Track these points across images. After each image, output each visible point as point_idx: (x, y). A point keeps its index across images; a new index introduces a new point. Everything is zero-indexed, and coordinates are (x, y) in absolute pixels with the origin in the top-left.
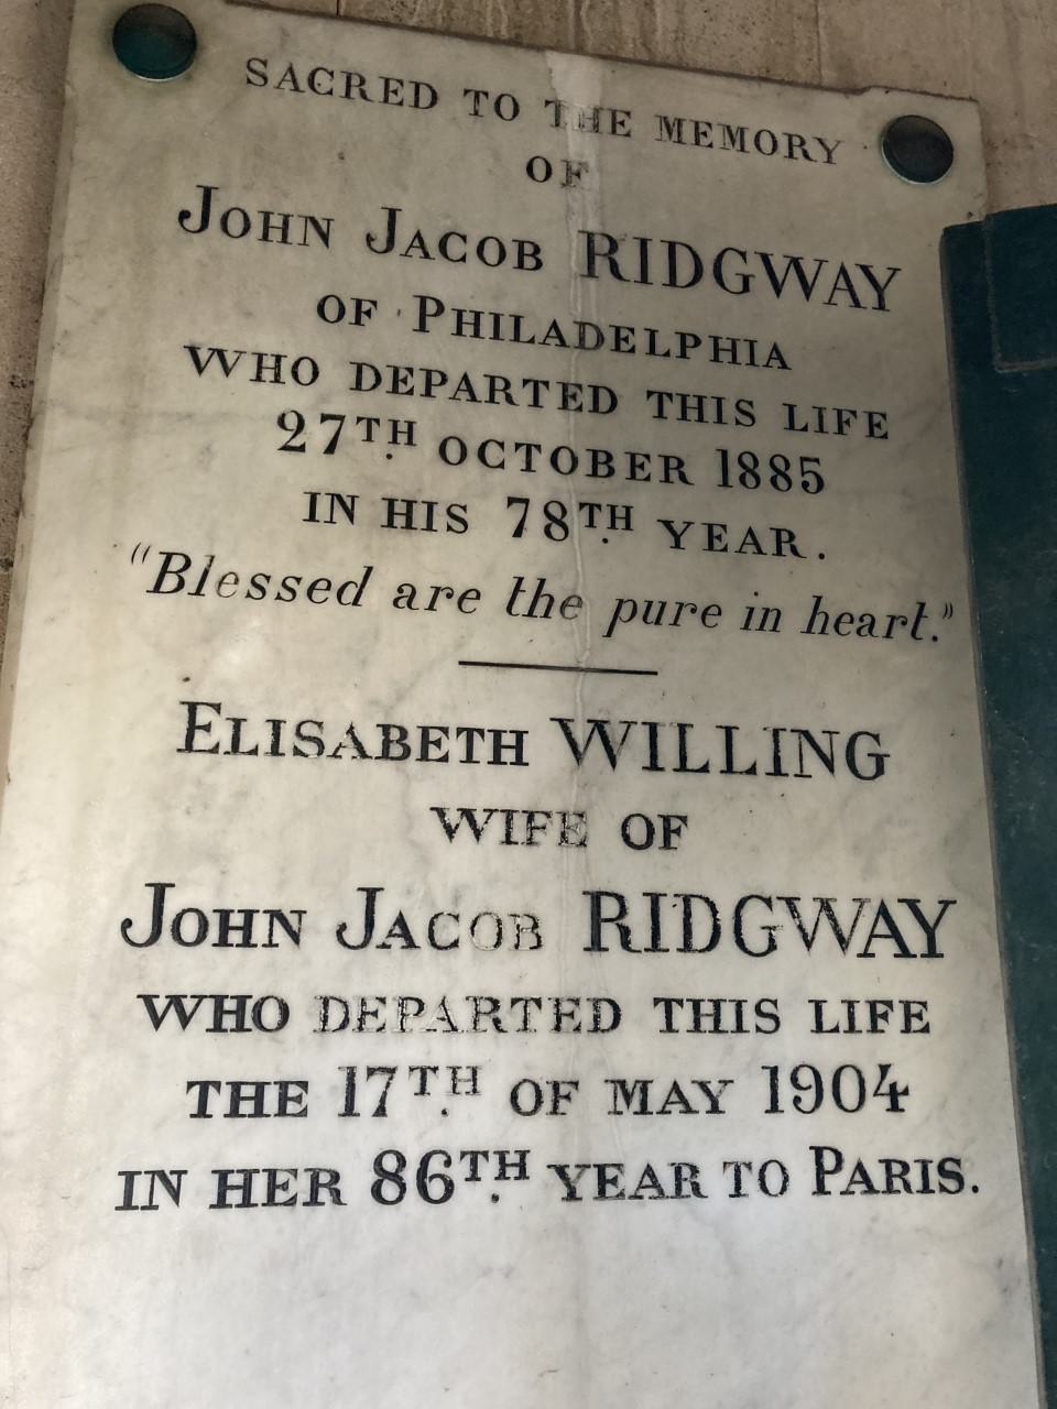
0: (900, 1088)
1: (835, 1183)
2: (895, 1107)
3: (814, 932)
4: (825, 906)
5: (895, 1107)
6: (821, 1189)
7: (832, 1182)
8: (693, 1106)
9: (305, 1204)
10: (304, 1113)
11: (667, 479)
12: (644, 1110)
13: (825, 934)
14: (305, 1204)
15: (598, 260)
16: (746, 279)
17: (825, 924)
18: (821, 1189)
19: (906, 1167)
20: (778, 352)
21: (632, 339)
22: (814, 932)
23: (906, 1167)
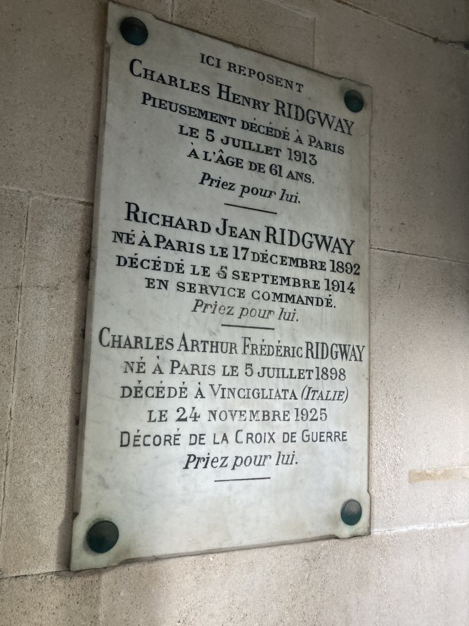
0: (198, 415)
1: (177, 371)
2: (352, 292)
3: (332, 122)
4: (327, 116)
5: (352, 292)
6: (172, 372)
7: (175, 370)
8: (343, 251)
9: (158, 421)
10: (166, 420)
11: (268, 241)
12: (293, 302)
13: (326, 123)
14: (158, 421)
15: (270, 236)
16: (314, 119)
17: (326, 120)
18: (172, 372)
19: (330, 145)
20: (300, 139)
21: (248, 277)
22: (332, 122)
23: (330, 145)
